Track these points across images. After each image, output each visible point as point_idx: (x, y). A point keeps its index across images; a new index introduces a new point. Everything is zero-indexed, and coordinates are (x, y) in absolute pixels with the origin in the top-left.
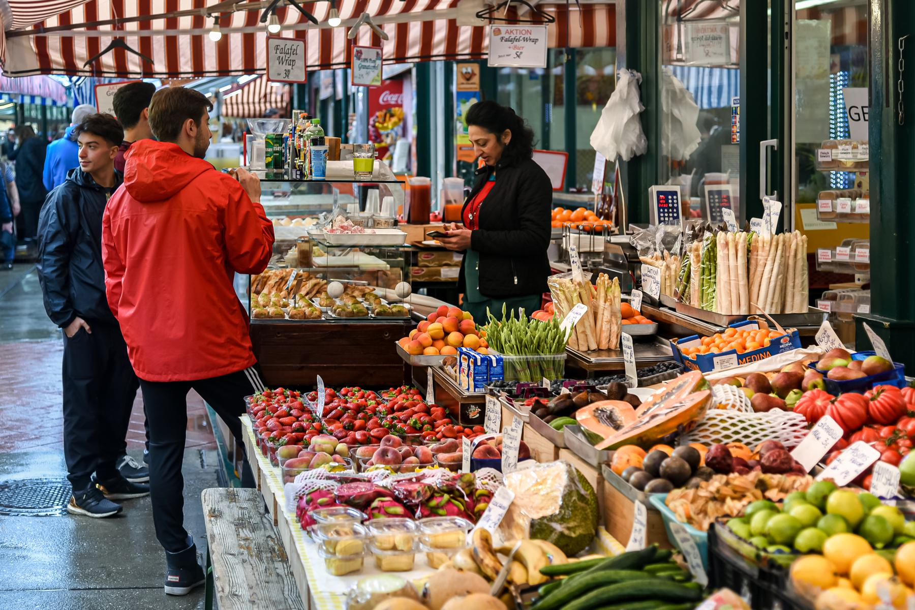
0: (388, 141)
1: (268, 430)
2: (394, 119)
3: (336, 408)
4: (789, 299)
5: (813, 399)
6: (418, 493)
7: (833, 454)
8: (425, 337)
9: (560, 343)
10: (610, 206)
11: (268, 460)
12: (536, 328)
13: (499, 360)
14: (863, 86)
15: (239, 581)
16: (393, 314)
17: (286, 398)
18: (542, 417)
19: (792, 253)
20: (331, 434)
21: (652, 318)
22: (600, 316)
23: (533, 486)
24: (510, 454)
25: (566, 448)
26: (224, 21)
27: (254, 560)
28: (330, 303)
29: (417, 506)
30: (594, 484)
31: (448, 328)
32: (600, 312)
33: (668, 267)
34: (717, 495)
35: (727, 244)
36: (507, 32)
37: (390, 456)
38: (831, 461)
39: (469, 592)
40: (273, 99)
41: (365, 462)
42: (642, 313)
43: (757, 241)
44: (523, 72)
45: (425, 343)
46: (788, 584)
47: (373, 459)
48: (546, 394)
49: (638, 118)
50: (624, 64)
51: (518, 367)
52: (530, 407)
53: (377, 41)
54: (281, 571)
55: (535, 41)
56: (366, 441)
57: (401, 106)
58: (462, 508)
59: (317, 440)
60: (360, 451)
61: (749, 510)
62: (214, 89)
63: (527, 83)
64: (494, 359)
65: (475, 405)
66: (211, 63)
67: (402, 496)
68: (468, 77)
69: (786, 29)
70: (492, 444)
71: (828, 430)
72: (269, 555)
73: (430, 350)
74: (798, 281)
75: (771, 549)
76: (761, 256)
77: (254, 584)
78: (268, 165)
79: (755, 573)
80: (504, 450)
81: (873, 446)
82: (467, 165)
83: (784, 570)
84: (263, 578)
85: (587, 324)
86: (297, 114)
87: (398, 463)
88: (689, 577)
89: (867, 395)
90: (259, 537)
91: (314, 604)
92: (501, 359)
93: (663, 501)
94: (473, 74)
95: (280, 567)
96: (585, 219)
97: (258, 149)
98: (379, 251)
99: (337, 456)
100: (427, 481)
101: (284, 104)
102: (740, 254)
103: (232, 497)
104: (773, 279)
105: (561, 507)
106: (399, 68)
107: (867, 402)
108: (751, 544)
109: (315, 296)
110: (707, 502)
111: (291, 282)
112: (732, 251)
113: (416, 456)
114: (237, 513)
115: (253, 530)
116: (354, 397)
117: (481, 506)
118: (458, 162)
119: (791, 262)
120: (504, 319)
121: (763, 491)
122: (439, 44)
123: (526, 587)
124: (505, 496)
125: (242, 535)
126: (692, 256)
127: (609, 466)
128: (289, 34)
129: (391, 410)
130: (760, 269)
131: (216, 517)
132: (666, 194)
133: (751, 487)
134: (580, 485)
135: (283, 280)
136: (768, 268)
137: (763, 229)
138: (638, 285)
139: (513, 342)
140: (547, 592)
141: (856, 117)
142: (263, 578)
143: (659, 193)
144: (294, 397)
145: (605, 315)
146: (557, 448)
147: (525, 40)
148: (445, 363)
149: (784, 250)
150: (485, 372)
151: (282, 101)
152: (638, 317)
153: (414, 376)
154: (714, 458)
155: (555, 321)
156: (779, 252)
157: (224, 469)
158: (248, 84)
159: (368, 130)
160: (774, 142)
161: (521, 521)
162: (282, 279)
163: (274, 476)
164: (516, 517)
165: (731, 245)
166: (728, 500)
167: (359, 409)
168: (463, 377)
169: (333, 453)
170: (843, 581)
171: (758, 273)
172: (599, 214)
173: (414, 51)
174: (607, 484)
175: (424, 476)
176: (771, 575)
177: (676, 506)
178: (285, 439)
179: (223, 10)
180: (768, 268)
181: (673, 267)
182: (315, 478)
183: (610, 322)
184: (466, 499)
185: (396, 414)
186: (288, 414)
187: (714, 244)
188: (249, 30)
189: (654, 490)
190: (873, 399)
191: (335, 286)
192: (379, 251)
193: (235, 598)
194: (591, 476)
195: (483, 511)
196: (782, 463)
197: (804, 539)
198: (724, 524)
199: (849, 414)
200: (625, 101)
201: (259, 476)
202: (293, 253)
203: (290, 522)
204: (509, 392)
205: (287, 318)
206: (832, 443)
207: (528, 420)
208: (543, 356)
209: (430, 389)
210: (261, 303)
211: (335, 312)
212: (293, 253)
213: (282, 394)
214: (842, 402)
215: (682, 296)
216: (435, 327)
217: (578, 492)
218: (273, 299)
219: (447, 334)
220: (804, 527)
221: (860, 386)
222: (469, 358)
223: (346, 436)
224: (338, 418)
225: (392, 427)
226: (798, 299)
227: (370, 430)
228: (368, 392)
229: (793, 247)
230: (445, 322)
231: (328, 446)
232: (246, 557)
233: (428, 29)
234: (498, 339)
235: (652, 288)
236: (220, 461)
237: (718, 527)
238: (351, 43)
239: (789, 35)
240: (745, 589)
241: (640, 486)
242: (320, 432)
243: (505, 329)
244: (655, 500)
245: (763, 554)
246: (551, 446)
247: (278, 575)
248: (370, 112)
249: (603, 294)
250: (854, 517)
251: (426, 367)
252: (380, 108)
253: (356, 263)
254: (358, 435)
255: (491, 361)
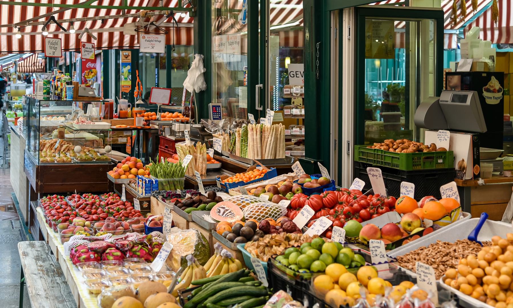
0: (90, 83)
1: (52, 215)
2: (93, 74)
3: (82, 204)
4: (278, 152)
5: (299, 197)
6: (128, 245)
7: (312, 222)
8: (121, 170)
9: (182, 173)
10: (188, 111)
11: (52, 230)
12: (172, 167)
13: (156, 181)
14: (301, 63)
15: (39, 287)
16: (103, 160)
17: (58, 199)
18: (180, 207)
19: (279, 133)
20: (81, 217)
21: (217, 160)
22: (198, 160)
23: (180, 241)
24: (167, 225)
25: (193, 222)
26: (22, 30)
27: (45, 276)
28: (75, 155)
29: (127, 251)
30: (208, 239)
31: (131, 167)
32: (198, 158)
33: (224, 139)
34: (268, 244)
35: (253, 129)
36: (148, 37)
37: (111, 227)
38: (311, 226)
39: (158, 293)
40: (38, 65)
41: (99, 230)
42: (214, 158)
43: (264, 128)
44: (147, 55)
45: (121, 173)
46: (311, 287)
47: (103, 228)
48: (179, 196)
49: (203, 75)
50: (197, 52)
51: (164, 184)
52: (174, 203)
53: (89, 40)
54: (58, 281)
55: (160, 42)
56: (98, 220)
57: (95, 68)
58: (147, 251)
59: (76, 220)
60: (96, 224)
61: (287, 252)
62: (14, 60)
63: (149, 59)
64: (154, 180)
65: (146, 201)
66: (15, 47)
67: (120, 247)
68: (126, 57)
69: (266, 39)
70: (157, 220)
71: (308, 211)
72: (52, 273)
73: (123, 177)
74: (281, 145)
75: (301, 271)
76: (266, 134)
77: (46, 288)
78: (44, 93)
79: (294, 283)
80: (164, 223)
81: (328, 218)
82: (126, 94)
83: (309, 281)
84: (51, 285)
85: (193, 164)
86: (56, 71)
87: (114, 230)
88: (260, 284)
89: (321, 195)
90: (46, 265)
91: (83, 303)
92: (157, 181)
93: (243, 247)
94: (129, 55)
95: (58, 279)
96: (178, 117)
97: (40, 86)
98: (94, 132)
99: (86, 227)
100: (130, 239)
101: (42, 67)
102: (258, 133)
103: (33, 246)
104: (272, 144)
105: (195, 250)
106: (97, 52)
107: (322, 199)
108: (291, 268)
109: (67, 152)
110: (264, 248)
111: (57, 145)
112: (255, 132)
113: (122, 226)
114: (35, 253)
115: (44, 261)
116: (90, 198)
117: (156, 250)
118: (122, 93)
119: (279, 136)
120: (157, 162)
121: (289, 241)
122: (116, 42)
123: (184, 290)
124: (168, 246)
125: (39, 264)
126: (237, 134)
127: (216, 231)
128: (51, 36)
129: (107, 204)
130: (266, 140)
131: (25, 255)
132: (216, 106)
133: (283, 240)
134: (202, 240)
135: (52, 145)
136: (269, 139)
137: (267, 122)
138: (212, 147)
139: (162, 173)
140: (196, 294)
141: (293, 76)
142: (51, 285)
143: (213, 106)
144: (61, 198)
145: (200, 160)
146: (188, 222)
147: (156, 41)
148: (130, 182)
149: (276, 132)
150: (150, 187)
151: (41, 65)
152: (213, 160)
153: (115, 188)
154: (263, 226)
155: (180, 163)
156: (274, 132)
157: (23, 229)
158: (27, 58)
159: (82, 78)
160: (261, 85)
161: (176, 257)
162: (52, 144)
163: (56, 237)
164: (174, 256)
165: (254, 129)
166: (274, 246)
167: (92, 204)
168: (140, 189)
169: (84, 226)
170: (336, 286)
171: (265, 142)
172: (184, 115)
173: (105, 44)
174: (214, 239)
175: (127, 237)
176: (302, 283)
177: (250, 250)
178: (60, 220)
179: (22, 25)
180: (269, 139)
181: (227, 138)
182: (77, 239)
183: (202, 163)
184: (149, 247)
185: (109, 206)
186: (60, 208)
187: (247, 128)
188: (33, 34)
189: (238, 242)
190: (324, 197)
191: (77, 148)
192: (94, 132)
193: (38, 296)
194: (206, 234)
195: (157, 252)
196: (292, 227)
197: (316, 265)
198: (275, 259)
199: (315, 204)
200: (197, 68)
201: (48, 237)
202: (55, 132)
203: (66, 260)
204: (163, 196)
205: (56, 162)
206: (310, 217)
207: (173, 209)
208: (175, 179)
209: (124, 194)
210: (44, 155)
211: (77, 159)
212: (55, 132)
213: (56, 197)
214: (312, 199)
215: (232, 151)
216: (125, 166)
217: (202, 243)
218: (48, 154)
219: (130, 169)
220: (314, 260)
221: (319, 190)
222: (143, 180)
223: (88, 218)
224: (83, 209)
225: (109, 213)
226: (281, 152)
227: (99, 214)
228: (95, 196)
229: (280, 130)
230: (130, 163)
231: (82, 223)
232: (41, 275)
233: (111, 35)
234: (155, 171)
235: (218, 147)
236: (21, 225)
237: (272, 260)
238: (78, 41)
239: (268, 41)
240: (288, 290)
241: (232, 240)
242: (76, 216)
243: (158, 167)
244: (239, 247)
245: (297, 273)
246: (185, 221)
247: (57, 283)
248: (82, 71)
249: (199, 151)
250: (335, 254)
251: (122, 184)
252: (87, 69)
253: (84, 137)
254: (94, 217)
255: (153, 181)
